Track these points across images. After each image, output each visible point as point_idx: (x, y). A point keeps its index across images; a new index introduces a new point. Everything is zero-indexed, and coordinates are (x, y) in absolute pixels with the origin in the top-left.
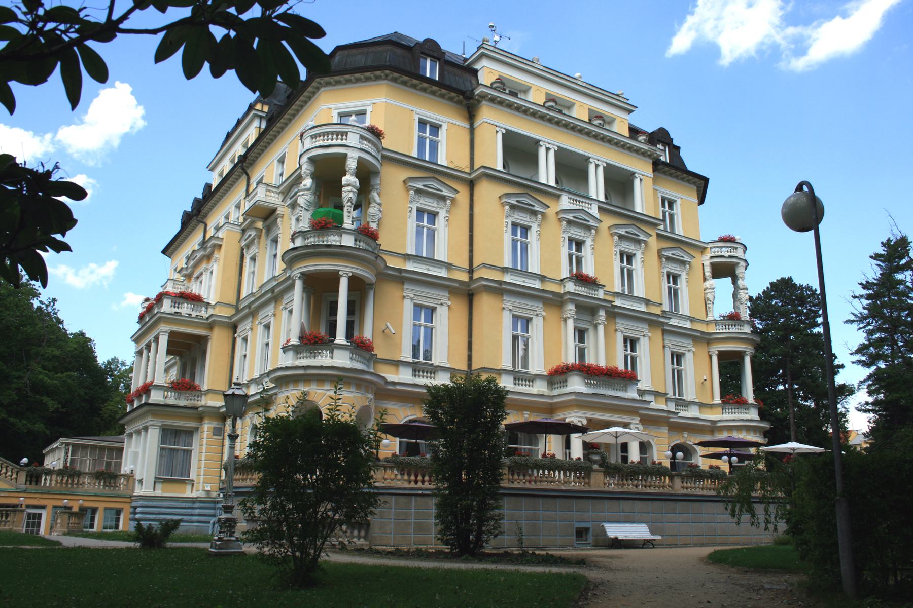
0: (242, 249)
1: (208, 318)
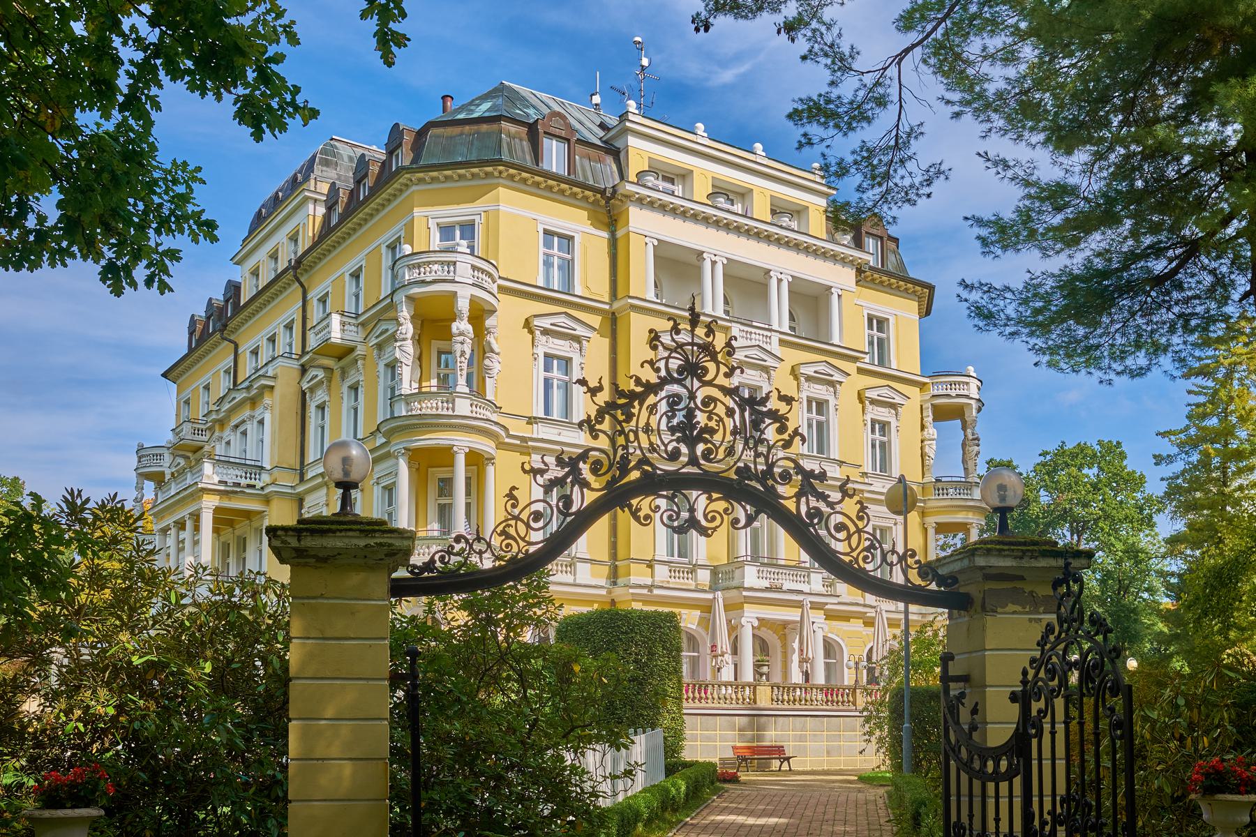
0: (304, 394)
1: (262, 488)
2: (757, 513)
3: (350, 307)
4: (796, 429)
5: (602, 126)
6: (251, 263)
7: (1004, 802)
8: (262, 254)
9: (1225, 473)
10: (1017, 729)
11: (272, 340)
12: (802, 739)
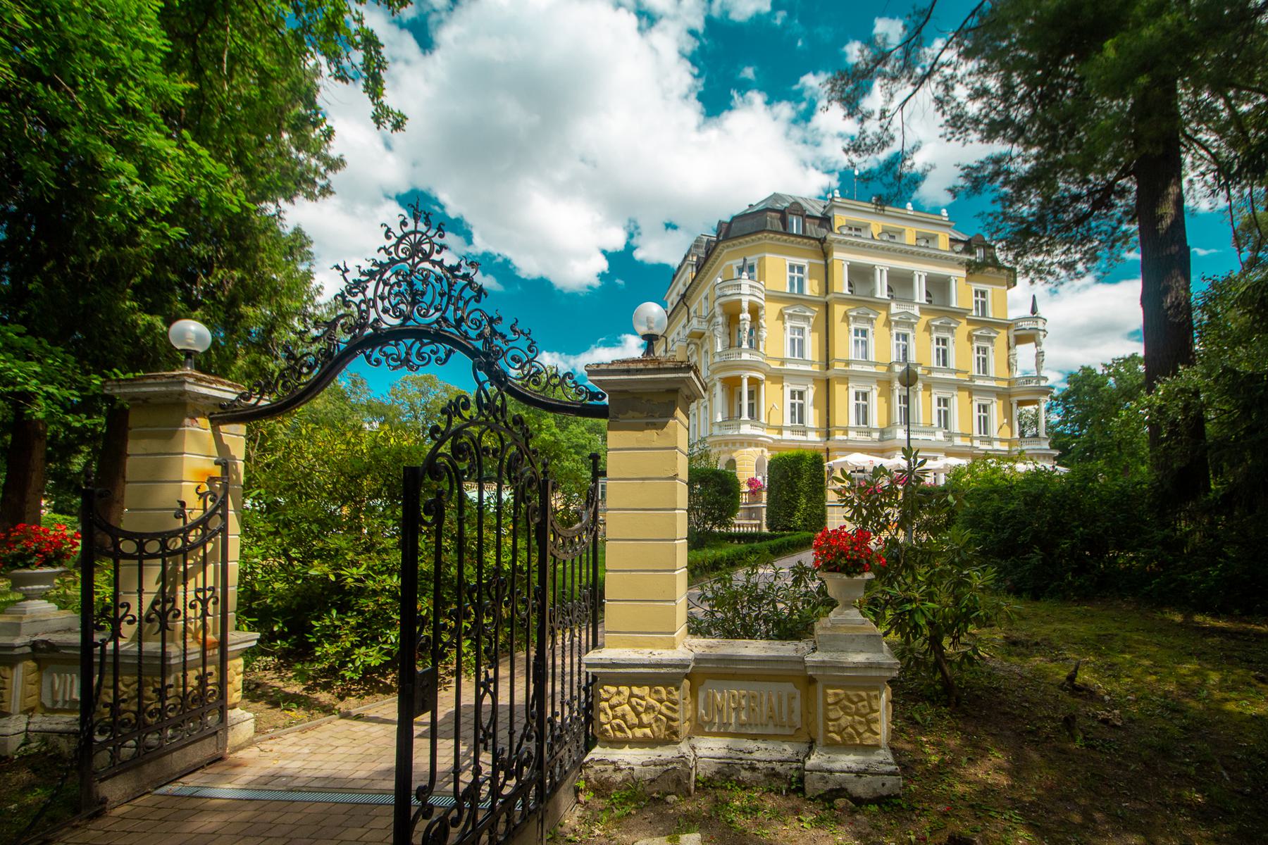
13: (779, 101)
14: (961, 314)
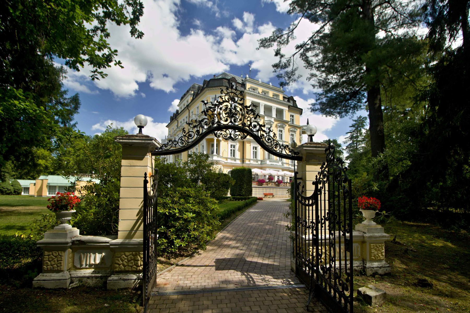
2: (247, 135)
3: (197, 113)
4: (258, 114)
5: (242, 80)
6: (180, 106)
7: (311, 212)
8: (182, 105)
9: (357, 145)
10: (314, 192)
11: (184, 120)
12: (277, 192)
13: (209, 35)
14: (287, 122)
